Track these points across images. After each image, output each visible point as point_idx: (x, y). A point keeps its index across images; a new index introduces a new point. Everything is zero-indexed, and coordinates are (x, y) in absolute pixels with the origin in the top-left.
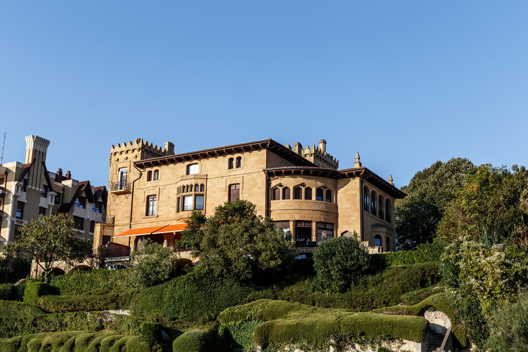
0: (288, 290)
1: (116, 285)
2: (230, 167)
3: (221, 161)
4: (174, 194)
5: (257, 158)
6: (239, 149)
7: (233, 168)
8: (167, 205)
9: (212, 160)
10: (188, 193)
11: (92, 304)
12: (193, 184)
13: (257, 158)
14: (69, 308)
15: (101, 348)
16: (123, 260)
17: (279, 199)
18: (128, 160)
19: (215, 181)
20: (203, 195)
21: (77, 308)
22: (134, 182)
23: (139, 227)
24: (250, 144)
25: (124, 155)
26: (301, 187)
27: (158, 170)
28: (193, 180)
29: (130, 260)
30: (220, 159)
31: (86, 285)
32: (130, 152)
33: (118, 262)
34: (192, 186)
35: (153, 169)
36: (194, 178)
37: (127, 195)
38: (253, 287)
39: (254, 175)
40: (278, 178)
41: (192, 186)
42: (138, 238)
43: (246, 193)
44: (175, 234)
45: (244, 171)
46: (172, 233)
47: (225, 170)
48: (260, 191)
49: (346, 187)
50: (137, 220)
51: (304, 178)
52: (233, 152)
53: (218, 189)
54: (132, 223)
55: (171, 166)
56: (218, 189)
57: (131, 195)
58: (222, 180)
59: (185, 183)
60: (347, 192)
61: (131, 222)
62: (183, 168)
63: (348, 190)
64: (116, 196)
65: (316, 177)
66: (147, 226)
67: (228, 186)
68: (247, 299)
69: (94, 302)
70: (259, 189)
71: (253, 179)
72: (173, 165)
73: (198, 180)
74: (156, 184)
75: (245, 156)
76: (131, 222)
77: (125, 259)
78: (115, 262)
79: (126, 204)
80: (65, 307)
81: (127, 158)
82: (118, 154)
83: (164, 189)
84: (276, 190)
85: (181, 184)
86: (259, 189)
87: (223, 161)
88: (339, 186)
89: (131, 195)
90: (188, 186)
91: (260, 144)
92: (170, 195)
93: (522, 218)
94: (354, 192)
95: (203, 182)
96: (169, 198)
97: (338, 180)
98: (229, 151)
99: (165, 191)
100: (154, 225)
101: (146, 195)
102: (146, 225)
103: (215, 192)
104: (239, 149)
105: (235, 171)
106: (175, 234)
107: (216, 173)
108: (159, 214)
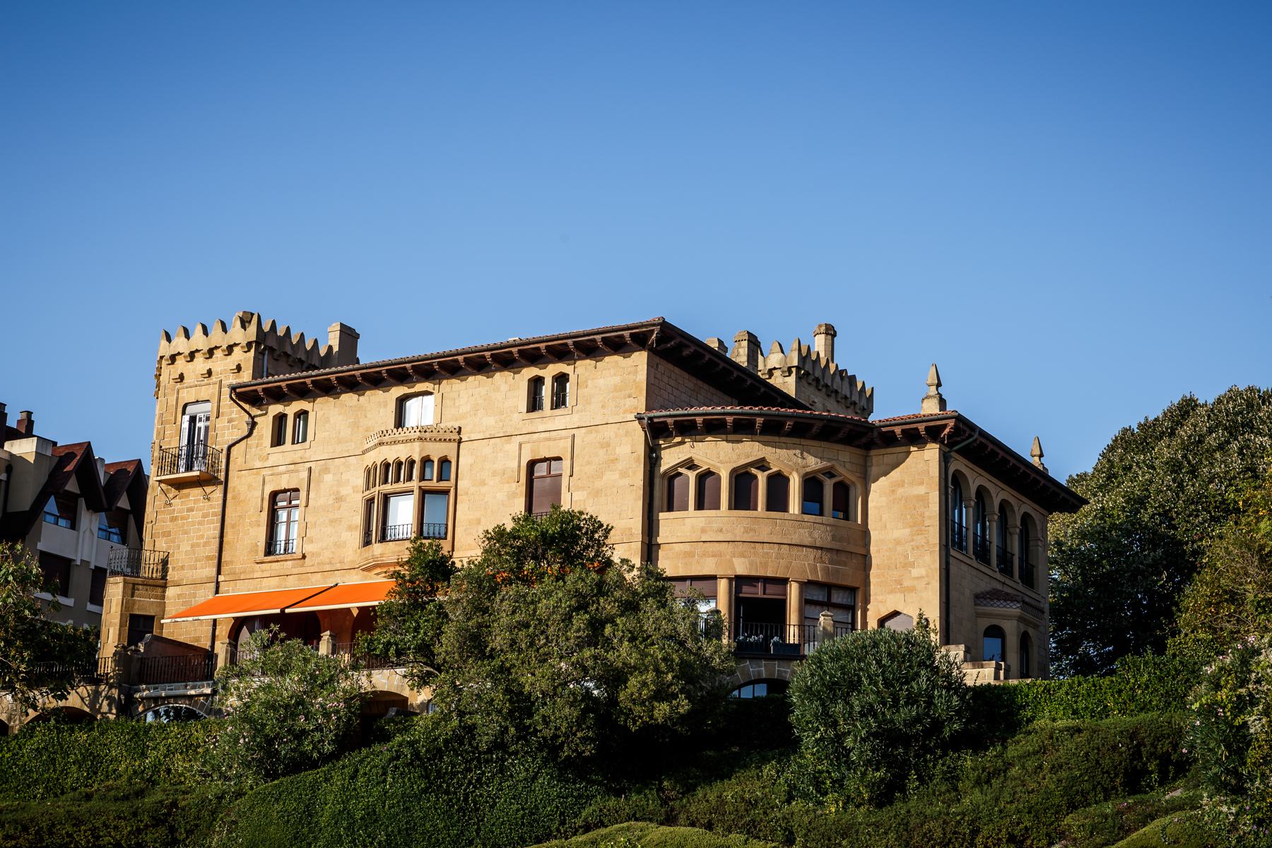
0: (707, 796)
1: (169, 771)
2: (534, 404)
3: (504, 388)
4: (355, 489)
6: (561, 350)
8: (331, 521)
9: (475, 383)
10: (401, 486)
11: (94, 830)
12: (417, 458)
16: (193, 692)
17: (717, 506)
18: (214, 379)
19: (486, 448)
20: (446, 492)
24: (628, 328)
25: (200, 364)
26: (754, 471)
27: (305, 413)
28: (417, 444)
29: (215, 692)
30: (502, 379)
31: (74, 768)
35: (550, 372)
36: (420, 439)
37: (208, 489)
38: (600, 783)
39: (609, 432)
40: (682, 443)
41: (412, 463)
42: (239, 624)
43: (583, 488)
45: (575, 420)
47: (516, 415)
48: (626, 482)
49: (895, 474)
50: (238, 566)
51: (765, 444)
52: (543, 360)
53: (494, 474)
55: (348, 398)
56: (494, 474)
57: (217, 493)
60: (900, 491)
61: (219, 572)
64: (173, 492)
65: (803, 441)
66: (270, 585)
68: (579, 822)
71: (606, 445)
74: (300, 454)
75: (581, 370)
76: (219, 572)
77: (198, 691)
78: (168, 697)
79: (204, 516)
85: (377, 457)
88: (874, 470)
89: (221, 488)
94: (921, 490)
95: (448, 450)
97: (873, 452)
98: (531, 354)
99: (328, 478)
100: (292, 584)
103: (483, 483)
105: (549, 419)
107: (489, 423)
108: (308, 549)
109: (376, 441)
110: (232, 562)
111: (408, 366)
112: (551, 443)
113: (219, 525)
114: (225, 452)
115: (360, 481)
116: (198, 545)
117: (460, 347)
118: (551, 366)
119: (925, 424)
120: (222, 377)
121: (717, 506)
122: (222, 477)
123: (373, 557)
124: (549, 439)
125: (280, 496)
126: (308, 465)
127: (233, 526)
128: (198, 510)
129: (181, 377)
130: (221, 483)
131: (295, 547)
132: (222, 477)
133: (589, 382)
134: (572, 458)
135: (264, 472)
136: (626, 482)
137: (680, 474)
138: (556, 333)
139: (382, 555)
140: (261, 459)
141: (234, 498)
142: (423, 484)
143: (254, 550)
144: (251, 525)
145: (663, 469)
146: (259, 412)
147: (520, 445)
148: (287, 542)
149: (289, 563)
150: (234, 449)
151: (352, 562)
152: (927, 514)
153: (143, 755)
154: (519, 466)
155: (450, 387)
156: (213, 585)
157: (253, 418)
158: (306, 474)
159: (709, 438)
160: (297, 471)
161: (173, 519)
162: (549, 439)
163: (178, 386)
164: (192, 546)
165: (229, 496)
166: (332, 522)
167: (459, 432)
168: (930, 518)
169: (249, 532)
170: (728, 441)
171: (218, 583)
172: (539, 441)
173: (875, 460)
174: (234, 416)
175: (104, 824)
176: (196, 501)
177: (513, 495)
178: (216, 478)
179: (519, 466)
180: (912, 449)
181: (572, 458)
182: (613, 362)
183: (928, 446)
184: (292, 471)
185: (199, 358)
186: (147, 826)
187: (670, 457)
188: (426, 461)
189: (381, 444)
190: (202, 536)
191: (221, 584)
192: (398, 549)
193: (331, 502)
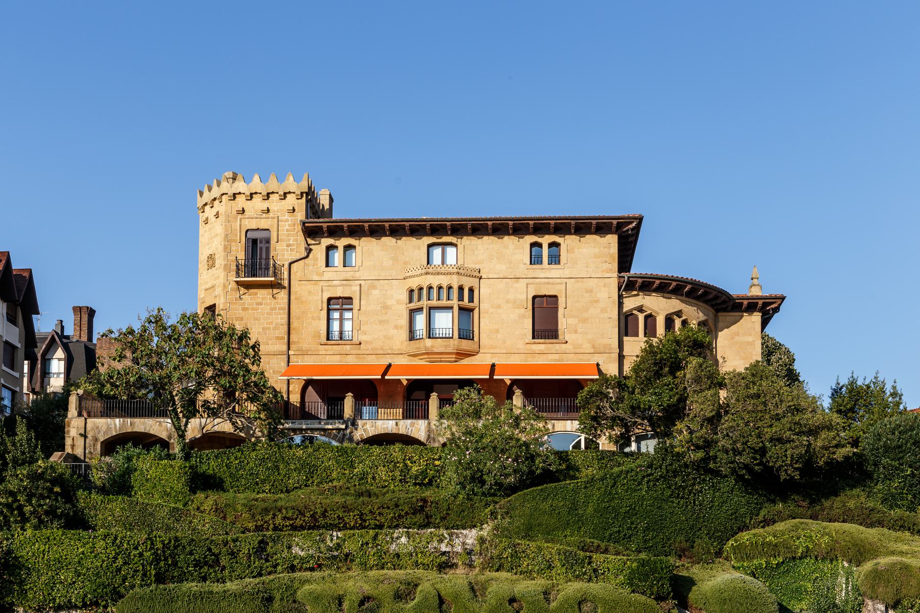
0: (835, 504)
2: (535, 260)
3: (511, 246)
4: (399, 302)
5: (597, 250)
6: (563, 227)
7: (541, 263)
8: (381, 322)
9: (489, 242)
11: (361, 515)
12: (445, 286)
13: (597, 250)
14: (298, 522)
15: (346, 605)
16: (330, 427)
17: (636, 334)
18: (271, 214)
20: (472, 310)
21: (322, 521)
22: (290, 264)
23: (309, 361)
24: (490, 220)
25: (258, 203)
26: (675, 317)
27: (354, 247)
28: (455, 277)
29: (347, 427)
30: (510, 241)
34: (430, 288)
36: (458, 273)
37: (275, 291)
38: (765, 496)
39: (592, 283)
40: (637, 295)
41: (421, 289)
43: (574, 317)
44: (405, 383)
45: (567, 273)
47: (522, 266)
48: (606, 315)
49: (734, 328)
50: (305, 346)
51: (682, 301)
52: (544, 231)
53: (508, 301)
54: (291, 352)
55: (388, 241)
56: (508, 301)
57: (282, 295)
58: (516, 285)
59: (425, 281)
60: (737, 338)
61: (289, 349)
62: (419, 248)
64: (243, 290)
65: (699, 303)
66: (334, 360)
67: (530, 298)
68: (760, 518)
69: (366, 511)
70: (603, 310)
71: (590, 291)
72: (393, 240)
74: (351, 274)
75: (568, 242)
76: (289, 349)
77: (334, 427)
78: (307, 429)
79: (272, 309)
80: (284, 518)
82: (241, 200)
85: (414, 283)
87: (516, 248)
88: (720, 325)
89: (286, 291)
91: (387, 225)
92: (389, 303)
95: (473, 282)
96: (386, 307)
97: (720, 314)
98: (540, 227)
99: (375, 292)
100: (351, 360)
101: (326, 296)
102: (334, 362)
103: (499, 307)
104: (563, 227)
105: (546, 270)
106: (405, 383)
107: (501, 268)
110: (298, 342)
113: (286, 316)
114: (286, 266)
115: (405, 296)
116: (269, 329)
117: (450, 217)
118: (547, 236)
121: (636, 334)
122: (286, 283)
124: (549, 283)
125: (332, 301)
127: (298, 318)
128: (266, 304)
130: (285, 288)
132: (286, 283)
133: (576, 250)
135: (322, 283)
136: (606, 315)
142: (460, 303)
144: (313, 318)
145: (624, 310)
146: (313, 242)
149: (348, 347)
150: (294, 266)
155: (467, 242)
156: (286, 356)
157: (309, 245)
158: (358, 288)
160: (350, 285)
161: (244, 309)
162: (549, 283)
165: (292, 297)
166: (381, 322)
169: (312, 323)
172: (541, 284)
173: (720, 318)
174: (291, 242)
175: (371, 512)
177: (523, 317)
178: (280, 284)
182: (592, 240)
184: (346, 285)
185: (257, 199)
186: (407, 513)
187: (630, 303)
188: (430, 288)
190: (272, 323)
191: (291, 357)
193: (379, 308)
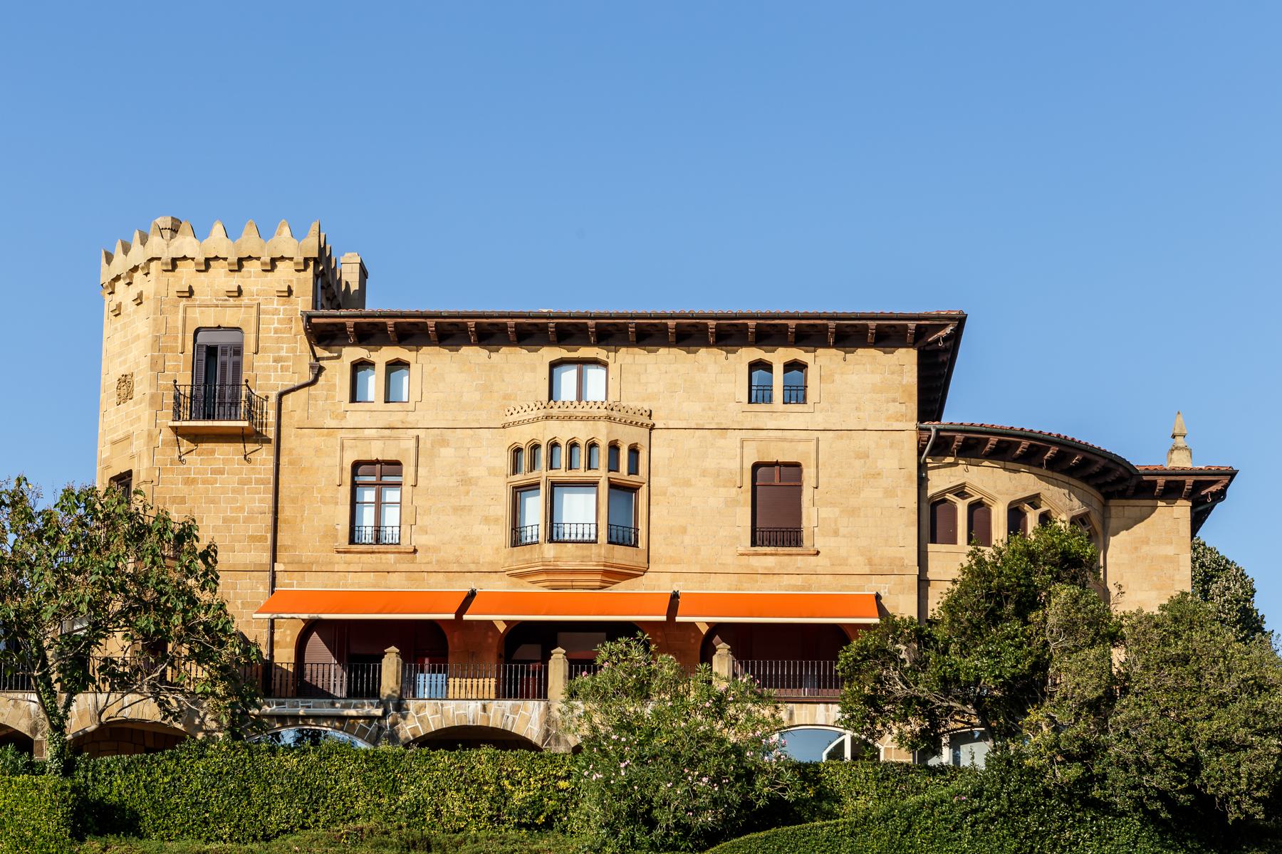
1: (437, 813)
4: (492, 472)
5: (877, 378)
10: (580, 473)
12: (582, 441)
13: (877, 378)
16: (352, 712)
17: (953, 541)
18: (245, 300)
19: (691, 441)
22: (281, 395)
23: (314, 583)
24: (671, 317)
25: (220, 278)
26: (1027, 507)
27: (406, 365)
30: (709, 357)
31: (282, 805)
32: (252, 267)
33: (317, 718)
35: (779, 357)
36: (609, 418)
37: (250, 447)
40: (955, 464)
41: (536, 447)
42: (312, 626)
44: (502, 628)
45: (819, 420)
46: (491, 623)
47: (732, 405)
50: (306, 555)
52: (777, 338)
53: (704, 473)
56: (704, 473)
57: (264, 454)
58: (721, 442)
59: (544, 433)
60: (1145, 549)
61: (274, 560)
62: (534, 369)
63: (1146, 541)
64: (186, 445)
65: (1073, 481)
73: (620, 427)
74: (400, 416)
76: (274, 560)
77: (361, 712)
79: (243, 482)
81: (240, 292)
82: (186, 270)
83: (444, 443)
84: (939, 508)
85: (523, 436)
86: (889, 493)
87: (723, 371)
88: (1113, 523)
89: (272, 447)
90: (573, 445)
92: (473, 472)
93: (180, 726)
94: (1170, 550)
95: (639, 436)
97: (1112, 502)
98: (769, 332)
99: (446, 452)
100: (396, 583)
103: (687, 483)
105: (779, 415)
107: (693, 410)
108: (419, 540)
109: (542, 413)
110: (294, 547)
111: (590, 322)
112: (786, 445)
116: (236, 520)
118: (781, 350)
119: (1195, 478)
120: (261, 299)
121: (953, 541)
122: (271, 433)
123: (544, 562)
124: (784, 440)
126: (416, 432)
129: (140, 296)
130: (269, 441)
131: (390, 533)
132: (271, 433)
133: (837, 377)
134: (417, 466)
137: (945, 501)
138: (849, 311)
139: (556, 559)
140: (335, 416)
141: (291, 463)
143: (331, 534)
144: (323, 501)
146: (326, 354)
147: (742, 441)
148: (378, 529)
150: (288, 401)
151: (492, 563)
152: (1177, 577)
153: (396, 791)
154: (742, 468)
155: (628, 359)
157: (317, 360)
159: (986, 463)
160: (398, 439)
162: (784, 440)
163: (184, 302)
164: (225, 520)
165: (284, 460)
166: (458, 510)
167: (650, 416)
168: (1181, 581)
170: (1005, 469)
171: (274, 572)
172: (770, 440)
173: (1114, 511)
176: (225, 461)
178: (259, 434)
179: (742, 468)
180: (1160, 503)
181: (417, 466)
182: (867, 357)
183: (1179, 502)
184: (389, 438)
185: (218, 269)
187: (940, 481)
189: (547, 418)
190: (241, 509)
192: (579, 553)
